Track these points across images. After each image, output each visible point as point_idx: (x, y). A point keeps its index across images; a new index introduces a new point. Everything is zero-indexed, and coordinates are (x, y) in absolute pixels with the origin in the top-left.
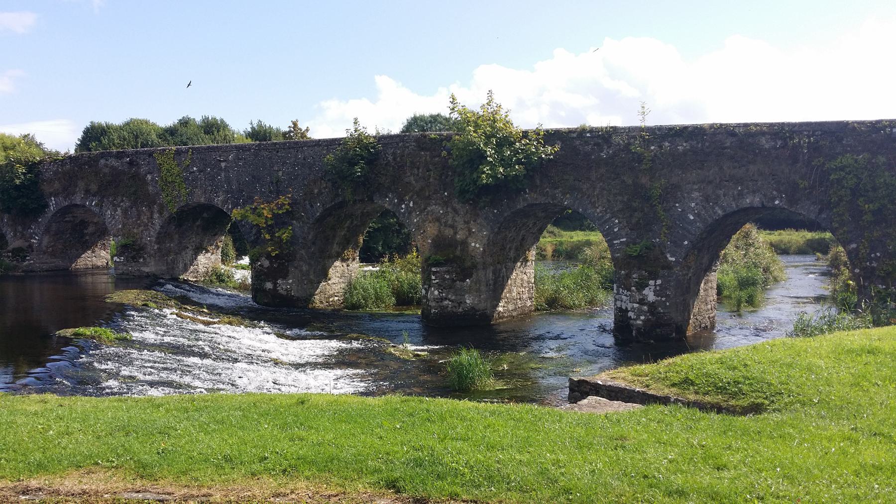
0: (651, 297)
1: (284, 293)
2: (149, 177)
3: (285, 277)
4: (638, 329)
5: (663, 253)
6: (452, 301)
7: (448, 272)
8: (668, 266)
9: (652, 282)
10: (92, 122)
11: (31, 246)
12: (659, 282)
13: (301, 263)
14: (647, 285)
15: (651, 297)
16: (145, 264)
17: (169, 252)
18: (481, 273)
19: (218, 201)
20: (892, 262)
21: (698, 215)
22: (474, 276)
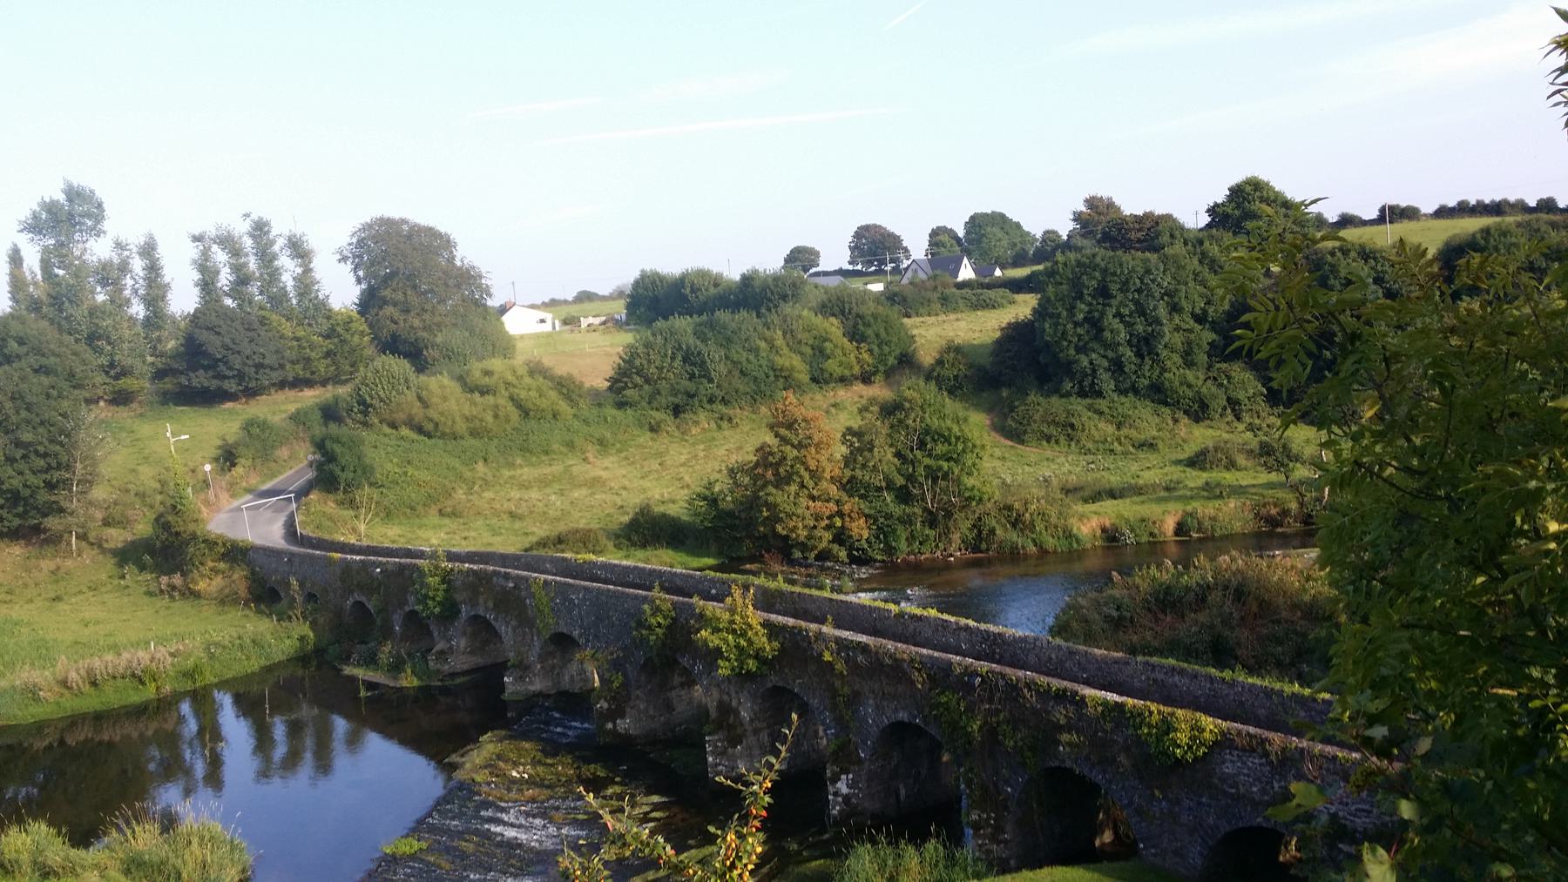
0: (845, 790)
1: (624, 732)
2: (528, 601)
3: (623, 716)
4: (835, 818)
5: (857, 749)
6: (726, 766)
7: (720, 740)
8: (860, 761)
9: (843, 777)
10: (642, 271)
11: (451, 648)
12: (851, 776)
13: (638, 702)
14: (840, 779)
15: (845, 790)
16: (531, 683)
17: (553, 667)
18: (752, 739)
19: (576, 633)
20: (1552, 681)
21: (873, 720)
22: (744, 742)
